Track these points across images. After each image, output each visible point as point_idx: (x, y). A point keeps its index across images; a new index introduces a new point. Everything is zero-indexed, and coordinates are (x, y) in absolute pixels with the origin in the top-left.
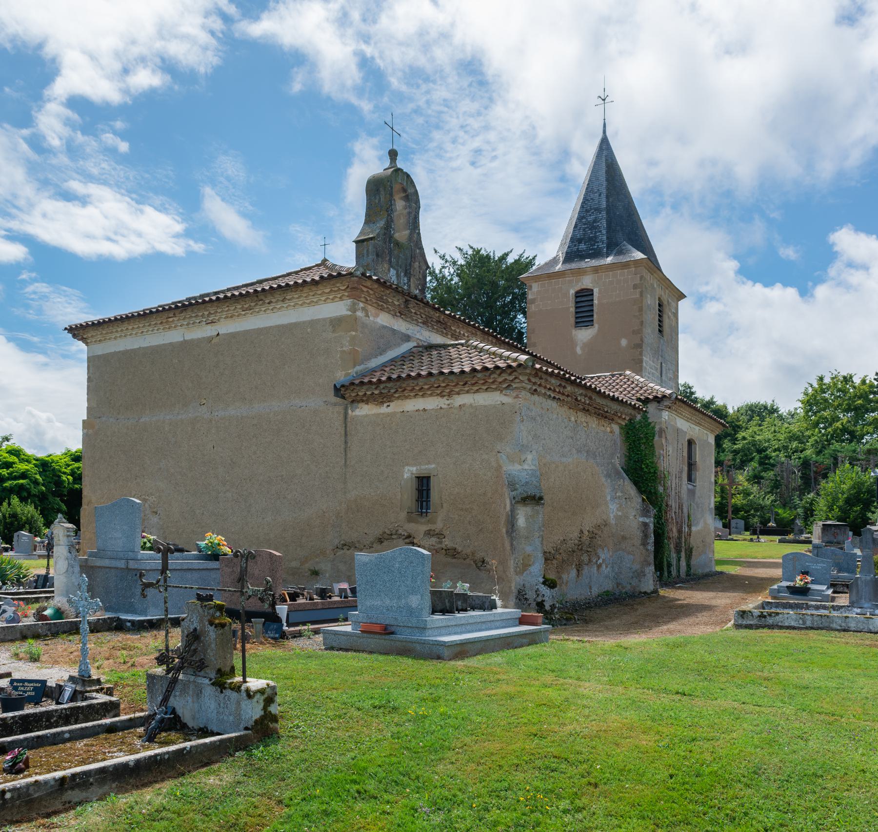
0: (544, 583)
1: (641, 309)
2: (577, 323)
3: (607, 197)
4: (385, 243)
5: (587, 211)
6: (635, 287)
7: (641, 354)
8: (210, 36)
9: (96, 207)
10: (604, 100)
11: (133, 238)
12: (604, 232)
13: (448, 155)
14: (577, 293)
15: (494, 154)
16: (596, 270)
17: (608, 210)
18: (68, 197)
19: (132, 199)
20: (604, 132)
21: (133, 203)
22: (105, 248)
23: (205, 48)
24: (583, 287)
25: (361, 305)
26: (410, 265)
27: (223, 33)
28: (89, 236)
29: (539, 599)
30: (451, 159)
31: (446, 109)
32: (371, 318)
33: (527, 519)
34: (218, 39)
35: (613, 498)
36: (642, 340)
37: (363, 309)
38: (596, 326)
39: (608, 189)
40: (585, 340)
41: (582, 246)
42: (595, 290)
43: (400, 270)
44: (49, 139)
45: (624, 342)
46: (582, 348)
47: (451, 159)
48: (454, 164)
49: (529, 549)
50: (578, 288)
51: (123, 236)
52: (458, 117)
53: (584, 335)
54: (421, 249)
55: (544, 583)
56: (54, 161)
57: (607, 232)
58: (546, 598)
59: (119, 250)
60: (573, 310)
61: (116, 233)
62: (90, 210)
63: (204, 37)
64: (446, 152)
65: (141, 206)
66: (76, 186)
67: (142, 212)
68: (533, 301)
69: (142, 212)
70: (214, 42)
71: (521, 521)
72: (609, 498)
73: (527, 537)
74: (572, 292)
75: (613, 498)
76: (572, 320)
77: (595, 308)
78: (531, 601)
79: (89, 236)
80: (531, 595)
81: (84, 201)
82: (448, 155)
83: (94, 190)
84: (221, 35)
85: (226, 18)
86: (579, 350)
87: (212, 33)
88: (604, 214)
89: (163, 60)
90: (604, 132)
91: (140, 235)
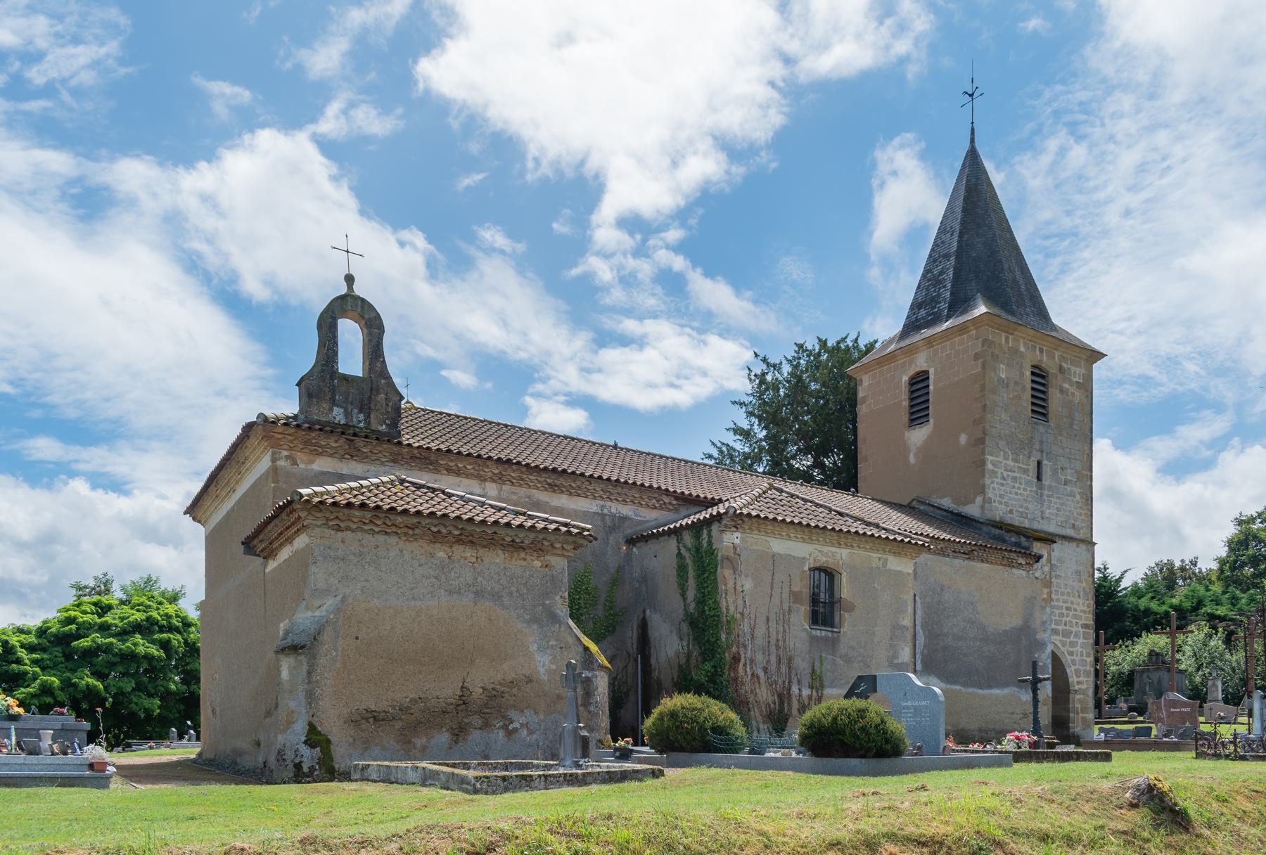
0: (305, 742)
1: (983, 388)
2: (912, 420)
3: (961, 235)
4: (324, 381)
5: (935, 261)
6: (977, 357)
7: (983, 453)
8: (769, 88)
9: (654, 348)
10: (971, 95)
11: (698, 379)
12: (949, 286)
13: (1091, 184)
14: (912, 378)
15: (1165, 164)
16: (929, 341)
17: (959, 254)
18: (624, 341)
19: (693, 329)
20: (972, 141)
21: (694, 333)
22: (668, 397)
23: (764, 107)
24: (918, 369)
25: (285, 453)
26: (370, 398)
27: (784, 80)
28: (651, 385)
29: (297, 761)
30: (1096, 188)
31: (1084, 117)
32: (302, 466)
33: (291, 674)
34: (780, 90)
35: (541, 649)
36: (984, 433)
37: (287, 457)
38: (932, 421)
39: (963, 223)
40: (919, 444)
41: (923, 312)
42: (932, 371)
43: (350, 407)
44: (600, 273)
45: (963, 439)
46: (916, 455)
47: (1096, 188)
48: (1101, 196)
49: (292, 704)
50: (912, 372)
51: (686, 378)
52: (1103, 125)
53: (918, 436)
54: (389, 378)
55: (305, 742)
56: (608, 301)
57: (953, 286)
58: (304, 759)
59: (682, 397)
60: (906, 403)
61: (678, 377)
62: (649, 353)
63: (764, 92)
64: (1088, 180)
65: (703, 337)
66: (630, 326)
67: (705, 343)
68: (864, 401)
69: (705, 343)
70: (776, 95)
71: (285, 674)
72: (535, 647)
73: (291, 692)
74: (905, 378)
75: (541, 649)
76: (905, 418)
77: (931, 397)
78: (289, 762)
79: (651, 385)
80: (289, 755)
81: (638, 342)
82: (1091, 184)
83: (650, 326)
84: (781, 84)
85: (788, 60)
86: (912, 459)
87: (772, 84)
88: (953, 260)
89: (715, 138)
90: (972, 141)
91: (704, 373)
